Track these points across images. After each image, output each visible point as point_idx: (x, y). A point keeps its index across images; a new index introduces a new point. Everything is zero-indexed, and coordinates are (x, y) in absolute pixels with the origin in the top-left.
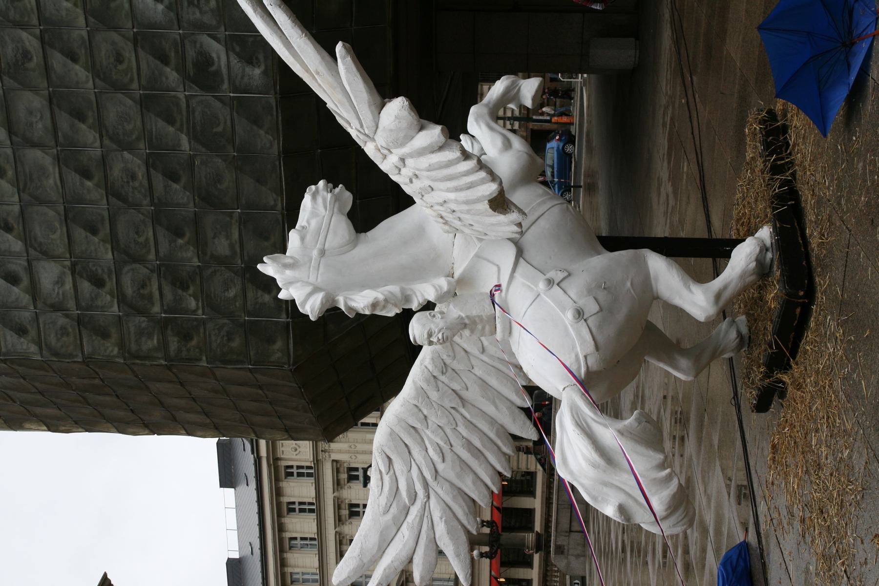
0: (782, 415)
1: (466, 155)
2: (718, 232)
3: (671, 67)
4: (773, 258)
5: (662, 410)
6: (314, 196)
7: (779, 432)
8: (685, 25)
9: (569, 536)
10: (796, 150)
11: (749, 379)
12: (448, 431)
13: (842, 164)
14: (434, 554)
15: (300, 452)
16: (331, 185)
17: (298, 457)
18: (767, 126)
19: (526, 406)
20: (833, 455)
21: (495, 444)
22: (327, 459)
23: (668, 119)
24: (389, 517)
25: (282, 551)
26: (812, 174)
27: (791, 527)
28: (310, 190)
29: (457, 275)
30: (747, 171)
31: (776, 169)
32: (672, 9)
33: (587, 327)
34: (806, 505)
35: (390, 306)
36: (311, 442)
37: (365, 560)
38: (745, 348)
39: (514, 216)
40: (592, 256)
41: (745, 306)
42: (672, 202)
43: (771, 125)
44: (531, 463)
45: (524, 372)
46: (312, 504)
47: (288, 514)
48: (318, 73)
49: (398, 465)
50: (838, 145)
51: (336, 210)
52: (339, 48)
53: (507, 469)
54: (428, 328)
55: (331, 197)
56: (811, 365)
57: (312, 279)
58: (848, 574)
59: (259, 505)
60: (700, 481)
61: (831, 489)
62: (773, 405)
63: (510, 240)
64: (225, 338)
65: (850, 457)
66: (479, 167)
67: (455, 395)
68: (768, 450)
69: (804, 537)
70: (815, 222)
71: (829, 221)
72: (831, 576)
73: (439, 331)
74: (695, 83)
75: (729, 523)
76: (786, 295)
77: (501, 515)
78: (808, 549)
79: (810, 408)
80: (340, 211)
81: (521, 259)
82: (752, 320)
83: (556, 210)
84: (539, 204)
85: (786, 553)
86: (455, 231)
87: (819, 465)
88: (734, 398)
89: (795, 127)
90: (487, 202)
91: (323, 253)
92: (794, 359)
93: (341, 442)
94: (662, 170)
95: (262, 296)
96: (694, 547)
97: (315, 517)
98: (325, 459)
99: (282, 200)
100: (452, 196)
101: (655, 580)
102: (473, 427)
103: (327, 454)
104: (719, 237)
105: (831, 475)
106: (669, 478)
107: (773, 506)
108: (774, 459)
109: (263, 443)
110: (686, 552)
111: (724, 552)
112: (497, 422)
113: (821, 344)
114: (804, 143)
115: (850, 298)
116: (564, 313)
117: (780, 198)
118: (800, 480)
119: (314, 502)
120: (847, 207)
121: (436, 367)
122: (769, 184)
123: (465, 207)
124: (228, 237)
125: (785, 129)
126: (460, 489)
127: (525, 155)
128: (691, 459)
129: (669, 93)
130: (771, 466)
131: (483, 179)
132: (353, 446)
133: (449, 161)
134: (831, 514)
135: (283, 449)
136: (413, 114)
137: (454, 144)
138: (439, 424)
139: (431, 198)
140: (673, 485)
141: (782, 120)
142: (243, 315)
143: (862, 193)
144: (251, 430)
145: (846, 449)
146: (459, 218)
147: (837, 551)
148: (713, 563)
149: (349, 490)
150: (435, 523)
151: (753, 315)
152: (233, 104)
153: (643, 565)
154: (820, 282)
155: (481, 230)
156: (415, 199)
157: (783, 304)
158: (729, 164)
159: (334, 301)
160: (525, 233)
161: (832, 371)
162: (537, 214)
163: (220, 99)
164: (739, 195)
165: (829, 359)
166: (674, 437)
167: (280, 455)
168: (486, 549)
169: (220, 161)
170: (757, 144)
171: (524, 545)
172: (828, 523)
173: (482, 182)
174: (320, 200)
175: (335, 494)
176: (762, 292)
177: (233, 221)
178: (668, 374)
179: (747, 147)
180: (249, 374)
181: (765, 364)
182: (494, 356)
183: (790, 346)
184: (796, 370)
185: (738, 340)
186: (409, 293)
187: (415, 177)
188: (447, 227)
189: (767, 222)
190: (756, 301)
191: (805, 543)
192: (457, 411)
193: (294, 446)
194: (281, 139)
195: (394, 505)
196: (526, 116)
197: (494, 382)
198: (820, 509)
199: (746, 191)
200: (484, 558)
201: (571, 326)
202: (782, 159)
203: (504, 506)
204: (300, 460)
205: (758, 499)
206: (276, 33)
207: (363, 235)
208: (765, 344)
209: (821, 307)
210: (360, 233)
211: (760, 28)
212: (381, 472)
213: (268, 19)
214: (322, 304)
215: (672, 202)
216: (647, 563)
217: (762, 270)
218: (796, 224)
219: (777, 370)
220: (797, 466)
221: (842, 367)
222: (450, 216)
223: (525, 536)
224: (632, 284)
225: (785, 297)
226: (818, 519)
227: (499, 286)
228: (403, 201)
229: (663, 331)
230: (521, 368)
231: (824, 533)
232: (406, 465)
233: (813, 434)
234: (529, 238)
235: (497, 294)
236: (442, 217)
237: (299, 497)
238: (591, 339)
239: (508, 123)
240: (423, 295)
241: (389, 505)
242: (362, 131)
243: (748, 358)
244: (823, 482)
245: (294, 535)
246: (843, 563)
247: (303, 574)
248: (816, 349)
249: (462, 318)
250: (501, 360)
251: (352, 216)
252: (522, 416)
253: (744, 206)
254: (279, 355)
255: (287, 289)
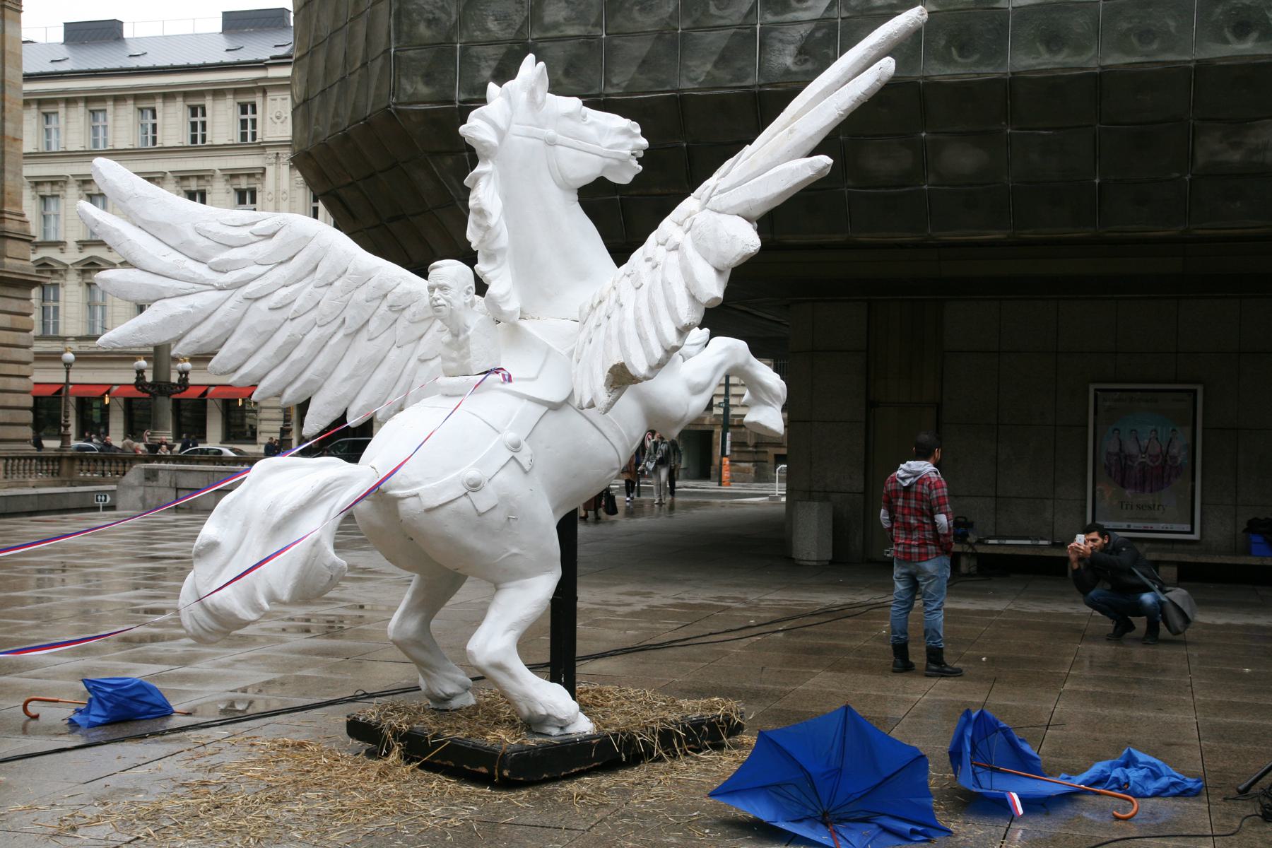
0: (345, 754)
1: (683, 331)
2: (582, 669)
3: (796, 605)
4: (551, 736)
5: (345, 604)
6: (626, 132)
7: (322, 751)
8: (849, 621)
9: (171, 487)
10: (691, 761)
11: (392, 711)
12: (313, 314)
13: (674, 818)
14: (141, 297)
15: (276, 123)
16: (641, 154)
17: (268, 119)
18: (722, 724)
19: (348, 419)
20: (294, 819)
21: (296, 379)
22: (268, 161)
23: (728, 603)
24: (192, 236)
25: (137, 98)
26: (661, 781)
27: (194, 769)
28: (634, 126)
29: (522, 323)
30: (664, 701)
31: (666, 737)
32: (869, 605)
33: (457, 496)
34: (225, 787)
35: (481, 234)
36: (289, 139)
37: (130, 204)
38: (432, 705)
39: (603, 397)
40: (552, 502)
41: (487, 704)
42: (621, 610)
43: (723, 729)
44: (269, 430)
45: (394, 415)
46: (204, 140)
47: (189, 106)
48: (791, 132)
49: (263, 248)
50: (698, 812)
51: (608, 161)
52: (825, 160)
53: (262, 396)
54: (451, 285)
55: (625, 155)
56: (411, 788)
57: (515, 128)
58: (135, 842)
59: (200, 66)
60: (251, 654)
61: (248, 817)
62: (357, 742)
63: (572, 393)
64: (431, 16)
65: (292, 840)
66: (669, 348)
67: (361, 324)
68: (298, 738)
69: (183, 785)
70: (599, 788)
71: (601, 804)
72: (131, 820)
73: (448, 301)
74: (775, 635)
75: (197, 692)
76: (503, 754)
77: (196, 397)
78: (165, 791)
79: (355, 789)
80: (607, 167)
81: (546, 409)
82: (470, 713)
83: (612, 454)
84: (618, 432)
85: (159, 764)
86: (581, 321)
87: (280, 801)
88: (365, 694)
89: (721, 759)
90: (622, 361)
91: (551, 143)
92: (420, 767)
93: (291, 179)
94: (664, 596)
95: (490, 66)
96: (163, 648)
97: (185, 145)
98: (266, 158)
99: (618, 94)
100: (629, 314)
101: (115, 600)
102: (319, 348)
103: (274, 161)
104: (578, 670)
105: (267, 817)
106: (256, 608)
107: (222, 746)
108: (285, 745)
109: (286, 72)
110: (154, 639)
111: (158, 686)
112: (326, 380)
113: (441, 799)
114: (700, 771)
115: (501, 834)
116: (475, 465)
117: (629, 743)
118: (259, 779)
119: (207, 143)
120: (618, 826)
121: (399, 297)
122: (647, 729)
123: (614, 332)
124: (568, 20)
125: (718, 746)
126: (233, 331)
127: (683, 413)
128: (281, 642)
129: (762, 603)
130: (276, 742)
131: (653, 355)
132: (285, 195)
133: (676, 309)
134: (215, 818)
135: (279, 100)
136: (738, 258)
137: (698, 317)
138: (321, 303)
139: (626, 289)
140: (246, 613)
141: (729, 742)
142: (463, 41)
143: (637, 843)
144: (305, 51)
145: (303, 834)
146: (600, 325)
147: (165, 827)
148: (140, 672)
149: (224, 191)
150: (186, 298)
151: (476, 714)
152: (746, 28)
153: (134, 584)
154: (521, 796)
155: (585, 353)
156: (624, 266)
157: (492, 750)
158: (672, 680)
159: (487, 158)
160: (580, 413)
161: (405, 814)
162: (604, 429)
163: (752, 10)
164: (632, 692)
165: (420, 810)
166: (308, 620)
167: (270, 95)
168: (149, 378)
169: (671, 10)
170: (699, 712)
171: (155, 429)
172: (202, 815)
173: (649, 354)
174: (622, 139)
175: (218, 172)
176: (507, 723)
177: (590, 28)
178: (392, 610)
179: (695, 701)
180: (381, 49)
181: (411, 730)
182: (415, 374)
183: (436, 761)
184: (404, 770)
185: (443, 695)
186: (499, 259)
187: (654, 265)
188: (587, 309)
189: (598, 727)
190: (495, 716)
191: (175, 787)
192: (340, 327)
193: (284, 115)
194: (700, 93)
195: (208, 242)
196: (730, 423)
197: (380, 375)
198: (221, 804)
199: (638, 700)
200: (135, 375)
201: (459, 476)
202: (680, 744)
203: (209, 402)
204: (263, 123)
205: (230, 727)
206: (844, 76)
207: (576, 198)
208: (439, 729)
209: (489, 798)
210: (578, 194)
211: (847, 708)
212: (253, 224)
213: (862, 65)
214: (481, 142)
215: (621, 610)
216: (137, 589)
217: (534, 724)
218: (596, 764)
219: (404, 745)
220: (277, 775)
221: (410, 827)
222: (603, 313)
223: (168, 429)
224: (516, 555)
225: (501, 752)
226: (207, 802)
227: (510, 380)
228: (620, 254)
229: (448, 603)
230: (401, 410)
231: (188, 811)
232: (263, 258)
233: (320, 794)
234: (572, 418)
235: (499, 377)
236: (600, 302)
237: (213, 122)
238: (441, 503)
239: (722, 400)
240: (495, 278)
241: (207, 235)
242: (714, 193)
243: (419, 709)
244: (257, 807)
245: (159, 115)
246: (149, 835)
247: (105, 127)
248: (433, 794)
249: (465, 331)
250: (410, 385)
251: (601, 183)
252: (335, 414)
253: (618, 699)
254: (410, 90)
255: (501, 95)
